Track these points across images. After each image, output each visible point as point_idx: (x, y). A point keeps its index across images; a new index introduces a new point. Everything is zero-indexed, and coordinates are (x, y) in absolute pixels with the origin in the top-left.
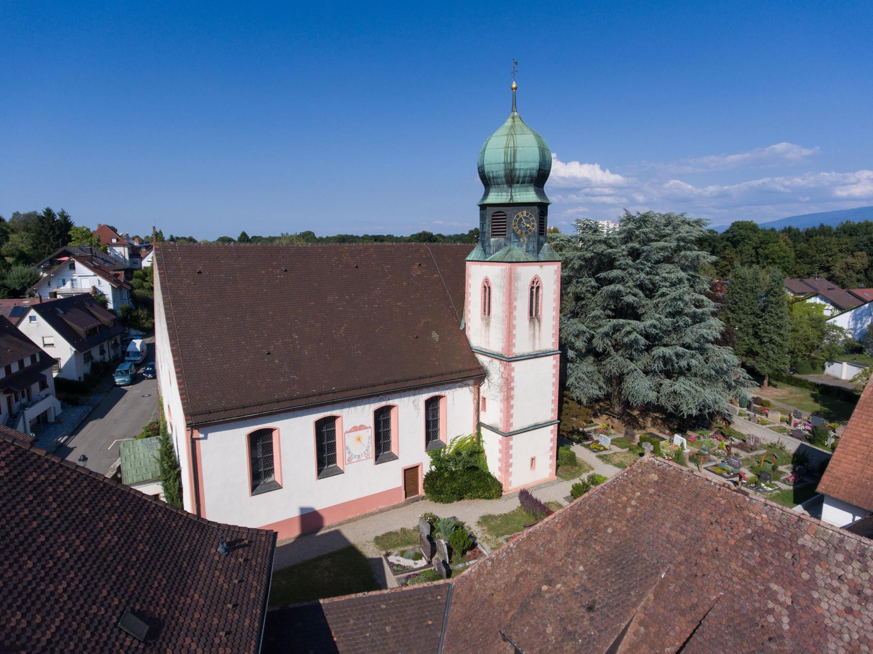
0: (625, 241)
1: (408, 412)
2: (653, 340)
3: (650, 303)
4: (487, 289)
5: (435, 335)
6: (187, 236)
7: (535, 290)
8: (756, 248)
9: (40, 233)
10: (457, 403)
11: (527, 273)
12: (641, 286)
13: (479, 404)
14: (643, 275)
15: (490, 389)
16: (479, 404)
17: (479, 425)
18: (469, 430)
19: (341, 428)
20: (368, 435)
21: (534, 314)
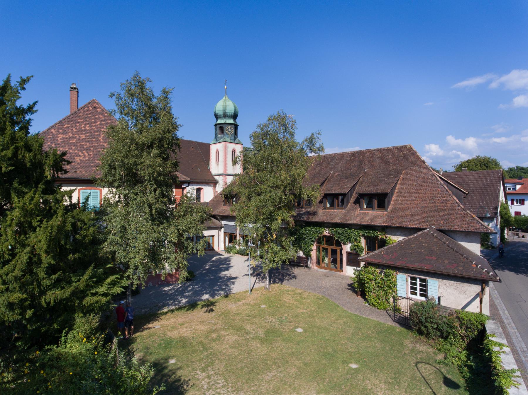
4: (217, 153)
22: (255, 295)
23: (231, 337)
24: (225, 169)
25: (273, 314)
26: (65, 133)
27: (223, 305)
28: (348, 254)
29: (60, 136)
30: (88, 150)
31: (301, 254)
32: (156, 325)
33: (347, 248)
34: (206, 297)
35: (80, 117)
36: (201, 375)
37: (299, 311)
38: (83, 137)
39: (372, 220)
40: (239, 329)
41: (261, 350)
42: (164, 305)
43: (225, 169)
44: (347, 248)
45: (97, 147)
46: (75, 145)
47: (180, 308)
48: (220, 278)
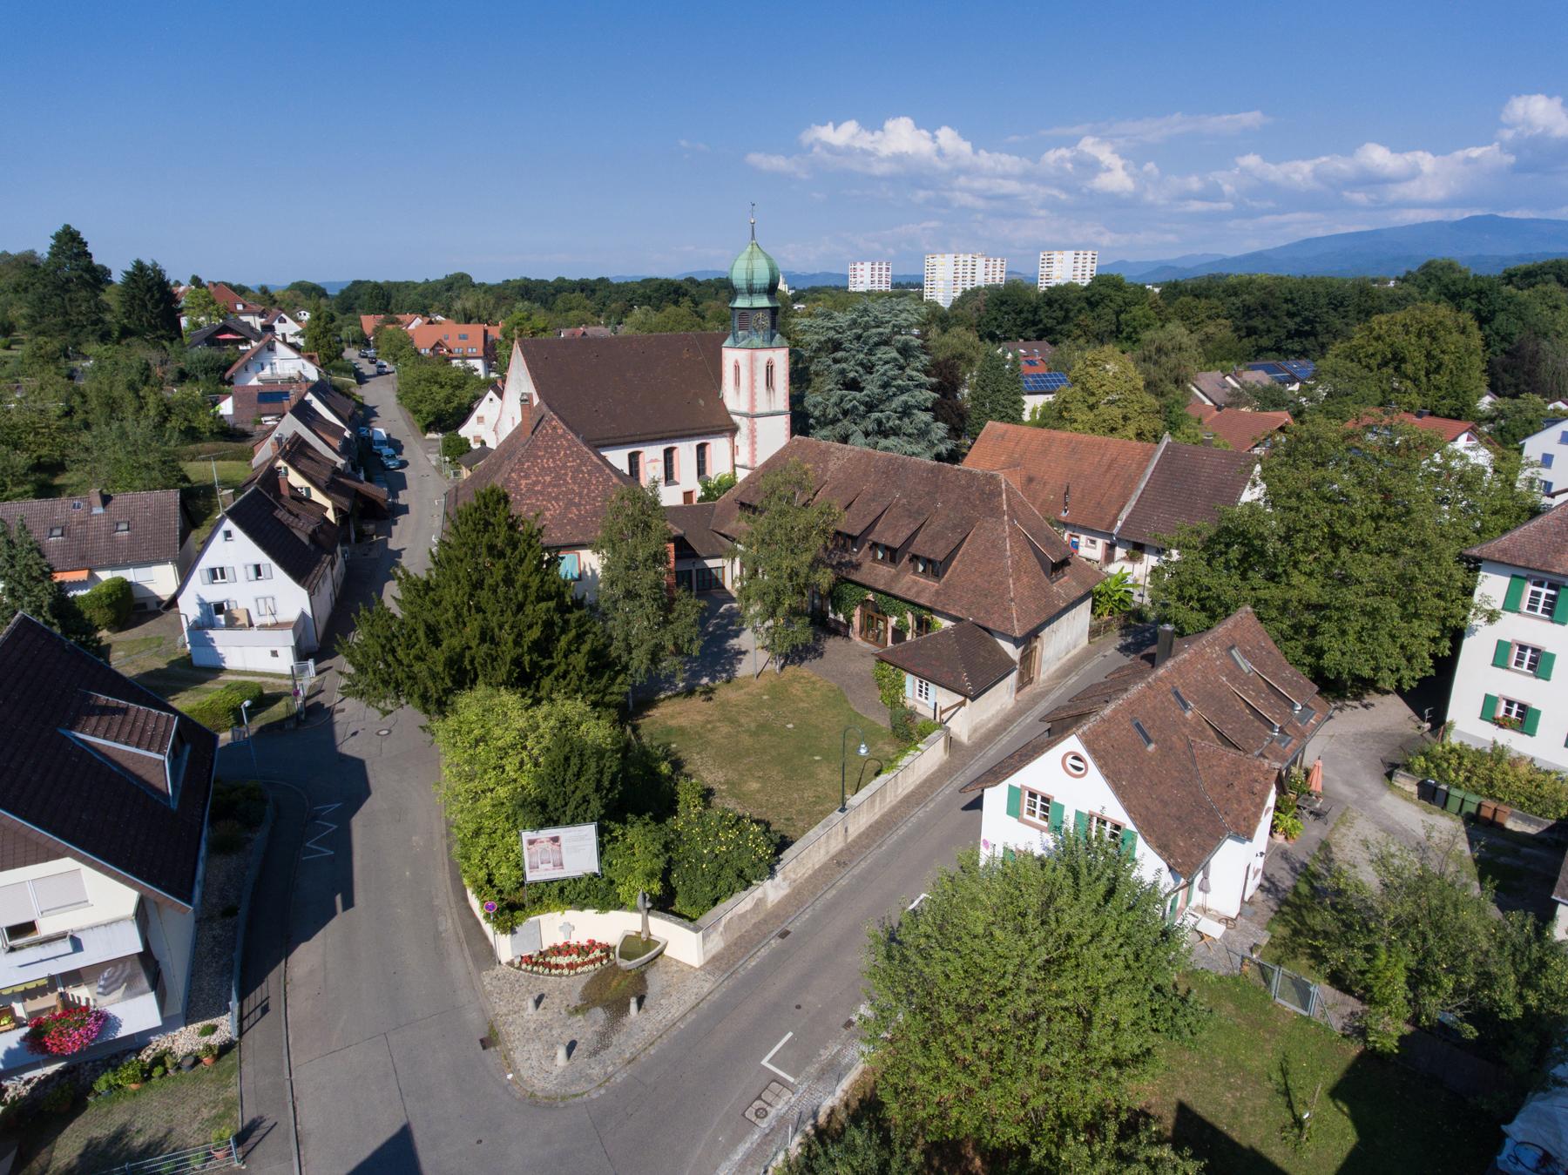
0: (850, 328)
1: (685, 452)
2: (871, 407)
3: (868, 377)
4: (737, 368)
5: (702, 402)
6: (235, 283)
7: (770, 369)
8: (1118, 314)
9: (133, 297)
10: (718, 448)
11: (764, 356)
12: (861, 364)
13: (734, 451)
14: (861, 356)
15: (741, 439)
16: (734, 451)
17: (734, 466)
18: (727, 470)
19: (643, 460)
20: (661, 465)
21: (769, 383)
22: (762, 681)
23: (725, 729)
24: (753, 405)
25: (771, 708)
26: (527, 477)
27: (724, 693)
28: (894, 630)
29: (523, 482)
30: (556, 499)
31: (841, 617)
32: (655, 713)
33: (893, 621)
34: (705, 680)
35: (539, 448)
36: (696, 756)
37: (802, 705)
38: (548, 479)
39: (918, 594)
40: (733, 721)
41: (747, 740)
42: (657, 693)
43: (753, 405)
44: (893, 621)
45: (566, 493)
46: (541, 493)
47: (678, 695)
48: (726, 651)
